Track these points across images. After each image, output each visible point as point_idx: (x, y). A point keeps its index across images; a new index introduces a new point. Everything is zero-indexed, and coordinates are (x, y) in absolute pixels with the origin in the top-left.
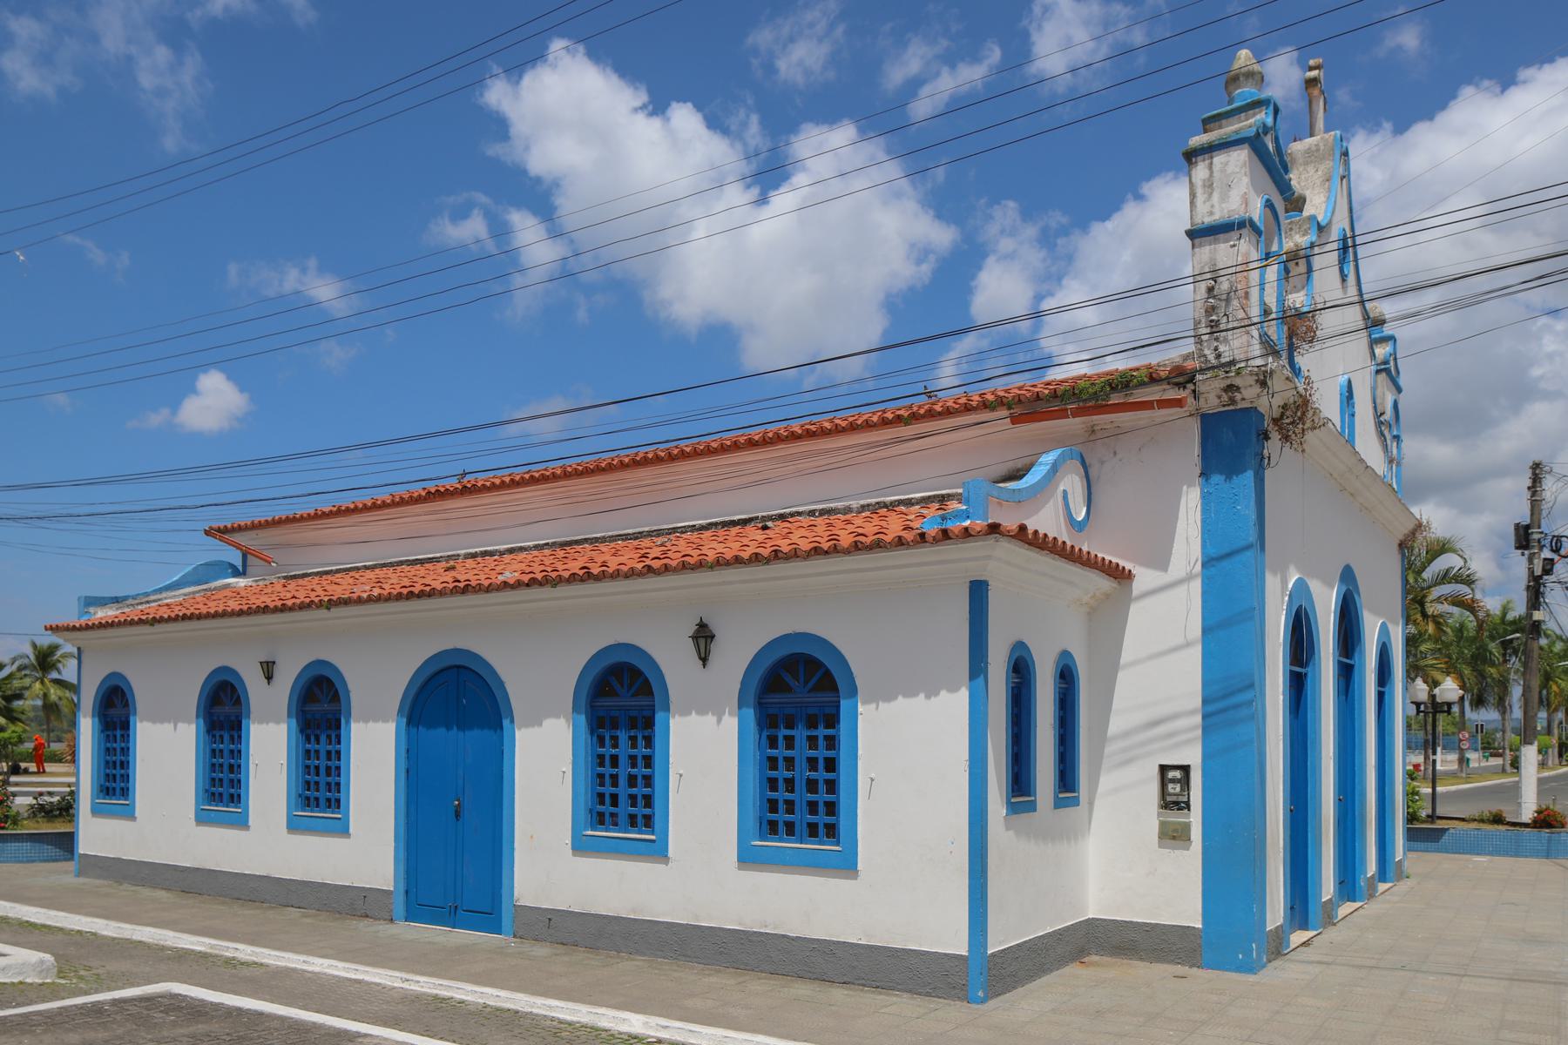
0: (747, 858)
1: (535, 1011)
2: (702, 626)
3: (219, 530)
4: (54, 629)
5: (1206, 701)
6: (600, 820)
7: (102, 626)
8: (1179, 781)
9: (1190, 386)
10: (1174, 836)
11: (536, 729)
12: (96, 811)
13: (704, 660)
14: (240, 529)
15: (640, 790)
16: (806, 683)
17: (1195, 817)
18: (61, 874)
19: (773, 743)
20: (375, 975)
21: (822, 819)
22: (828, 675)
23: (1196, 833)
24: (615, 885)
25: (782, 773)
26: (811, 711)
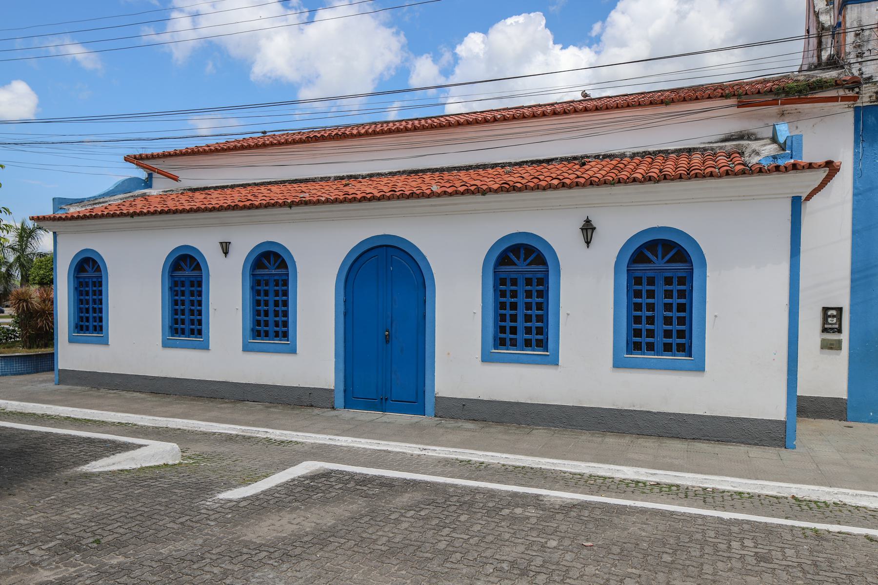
1: (543, 467)
2: (588, 221)
3: (135, 157)
4: (38, 219)
5: (853, 272)
6: (501, 343)
7: (72, 218)
8: (834, 316)
9: (857, 90)
10: (834, 346)
12: (71, 340)
13: (588, 243)
14: (153, 157)
15: (280, 319)
17: (845, 337)
18: (43, 381)
20: (396, 446)
22: (283, 261)
23: (845, 345)
24: (518, 381)
25: (263, 308)
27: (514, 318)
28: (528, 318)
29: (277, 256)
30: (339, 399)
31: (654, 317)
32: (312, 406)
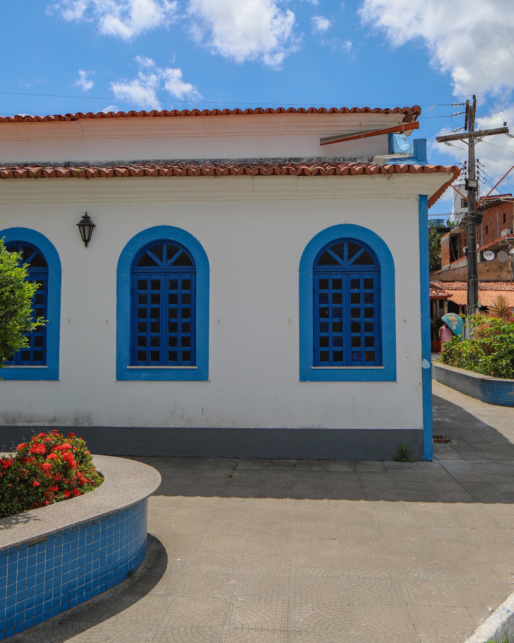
13: (86, 241)
31: (341, 323)
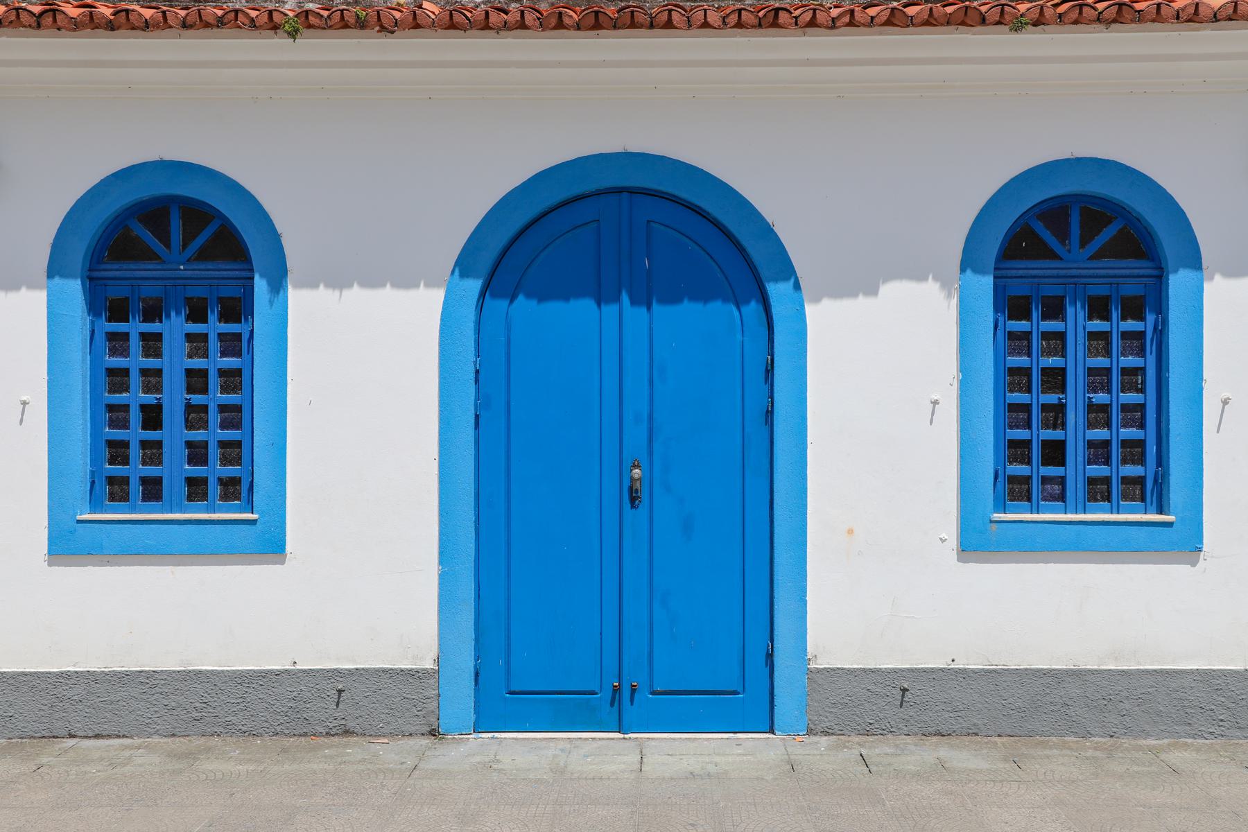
0: (975, 542)
6: (1016, 491)
11: (862, 302)
16: (1084, 243)
19: (118, 343)
21: (215, 469)
26: (196, 292)
27: (1055, 416)
28: (1099, 415)
29: (197, 215)
30: (460, 697)
32: (347, 732)
